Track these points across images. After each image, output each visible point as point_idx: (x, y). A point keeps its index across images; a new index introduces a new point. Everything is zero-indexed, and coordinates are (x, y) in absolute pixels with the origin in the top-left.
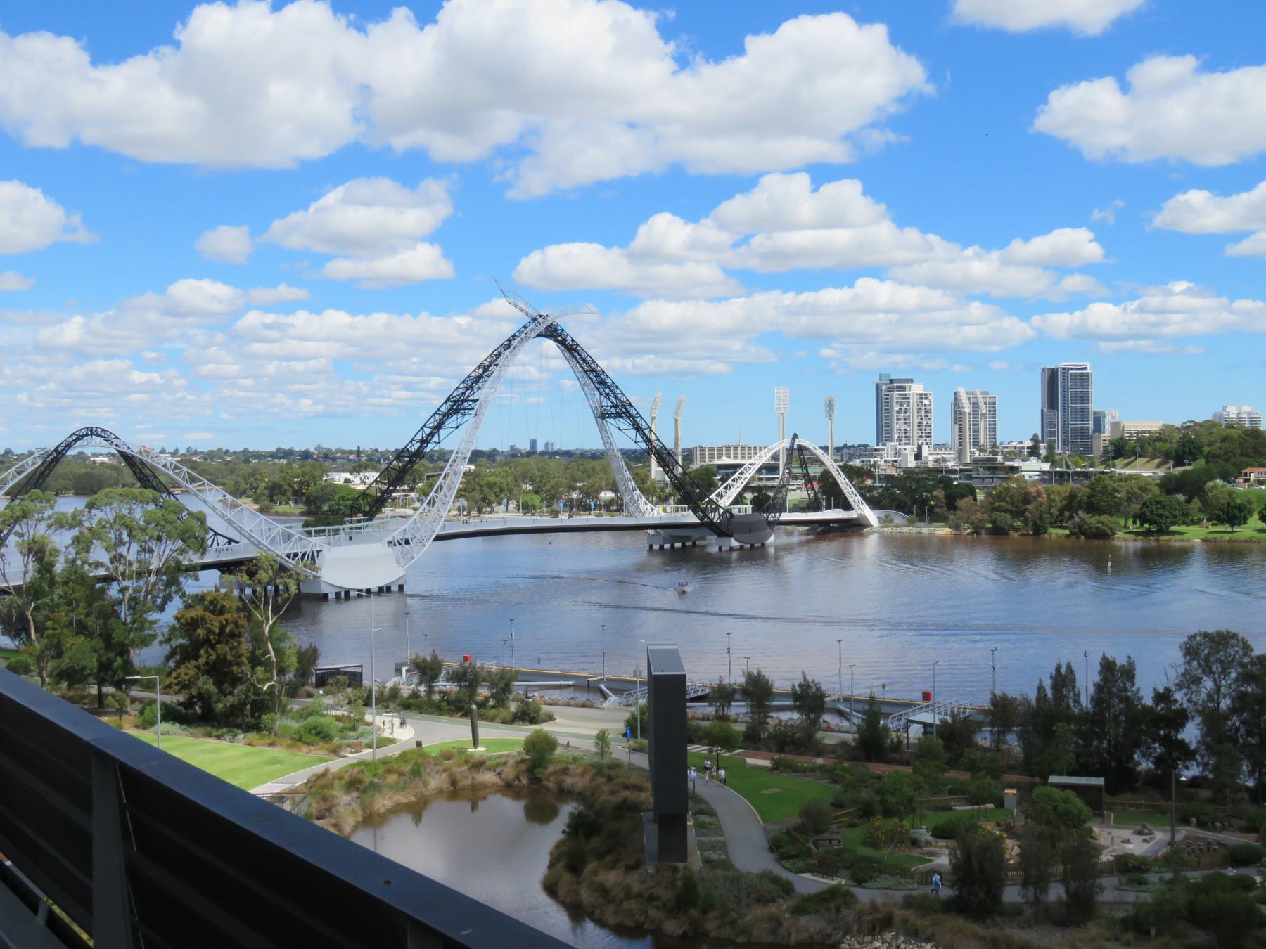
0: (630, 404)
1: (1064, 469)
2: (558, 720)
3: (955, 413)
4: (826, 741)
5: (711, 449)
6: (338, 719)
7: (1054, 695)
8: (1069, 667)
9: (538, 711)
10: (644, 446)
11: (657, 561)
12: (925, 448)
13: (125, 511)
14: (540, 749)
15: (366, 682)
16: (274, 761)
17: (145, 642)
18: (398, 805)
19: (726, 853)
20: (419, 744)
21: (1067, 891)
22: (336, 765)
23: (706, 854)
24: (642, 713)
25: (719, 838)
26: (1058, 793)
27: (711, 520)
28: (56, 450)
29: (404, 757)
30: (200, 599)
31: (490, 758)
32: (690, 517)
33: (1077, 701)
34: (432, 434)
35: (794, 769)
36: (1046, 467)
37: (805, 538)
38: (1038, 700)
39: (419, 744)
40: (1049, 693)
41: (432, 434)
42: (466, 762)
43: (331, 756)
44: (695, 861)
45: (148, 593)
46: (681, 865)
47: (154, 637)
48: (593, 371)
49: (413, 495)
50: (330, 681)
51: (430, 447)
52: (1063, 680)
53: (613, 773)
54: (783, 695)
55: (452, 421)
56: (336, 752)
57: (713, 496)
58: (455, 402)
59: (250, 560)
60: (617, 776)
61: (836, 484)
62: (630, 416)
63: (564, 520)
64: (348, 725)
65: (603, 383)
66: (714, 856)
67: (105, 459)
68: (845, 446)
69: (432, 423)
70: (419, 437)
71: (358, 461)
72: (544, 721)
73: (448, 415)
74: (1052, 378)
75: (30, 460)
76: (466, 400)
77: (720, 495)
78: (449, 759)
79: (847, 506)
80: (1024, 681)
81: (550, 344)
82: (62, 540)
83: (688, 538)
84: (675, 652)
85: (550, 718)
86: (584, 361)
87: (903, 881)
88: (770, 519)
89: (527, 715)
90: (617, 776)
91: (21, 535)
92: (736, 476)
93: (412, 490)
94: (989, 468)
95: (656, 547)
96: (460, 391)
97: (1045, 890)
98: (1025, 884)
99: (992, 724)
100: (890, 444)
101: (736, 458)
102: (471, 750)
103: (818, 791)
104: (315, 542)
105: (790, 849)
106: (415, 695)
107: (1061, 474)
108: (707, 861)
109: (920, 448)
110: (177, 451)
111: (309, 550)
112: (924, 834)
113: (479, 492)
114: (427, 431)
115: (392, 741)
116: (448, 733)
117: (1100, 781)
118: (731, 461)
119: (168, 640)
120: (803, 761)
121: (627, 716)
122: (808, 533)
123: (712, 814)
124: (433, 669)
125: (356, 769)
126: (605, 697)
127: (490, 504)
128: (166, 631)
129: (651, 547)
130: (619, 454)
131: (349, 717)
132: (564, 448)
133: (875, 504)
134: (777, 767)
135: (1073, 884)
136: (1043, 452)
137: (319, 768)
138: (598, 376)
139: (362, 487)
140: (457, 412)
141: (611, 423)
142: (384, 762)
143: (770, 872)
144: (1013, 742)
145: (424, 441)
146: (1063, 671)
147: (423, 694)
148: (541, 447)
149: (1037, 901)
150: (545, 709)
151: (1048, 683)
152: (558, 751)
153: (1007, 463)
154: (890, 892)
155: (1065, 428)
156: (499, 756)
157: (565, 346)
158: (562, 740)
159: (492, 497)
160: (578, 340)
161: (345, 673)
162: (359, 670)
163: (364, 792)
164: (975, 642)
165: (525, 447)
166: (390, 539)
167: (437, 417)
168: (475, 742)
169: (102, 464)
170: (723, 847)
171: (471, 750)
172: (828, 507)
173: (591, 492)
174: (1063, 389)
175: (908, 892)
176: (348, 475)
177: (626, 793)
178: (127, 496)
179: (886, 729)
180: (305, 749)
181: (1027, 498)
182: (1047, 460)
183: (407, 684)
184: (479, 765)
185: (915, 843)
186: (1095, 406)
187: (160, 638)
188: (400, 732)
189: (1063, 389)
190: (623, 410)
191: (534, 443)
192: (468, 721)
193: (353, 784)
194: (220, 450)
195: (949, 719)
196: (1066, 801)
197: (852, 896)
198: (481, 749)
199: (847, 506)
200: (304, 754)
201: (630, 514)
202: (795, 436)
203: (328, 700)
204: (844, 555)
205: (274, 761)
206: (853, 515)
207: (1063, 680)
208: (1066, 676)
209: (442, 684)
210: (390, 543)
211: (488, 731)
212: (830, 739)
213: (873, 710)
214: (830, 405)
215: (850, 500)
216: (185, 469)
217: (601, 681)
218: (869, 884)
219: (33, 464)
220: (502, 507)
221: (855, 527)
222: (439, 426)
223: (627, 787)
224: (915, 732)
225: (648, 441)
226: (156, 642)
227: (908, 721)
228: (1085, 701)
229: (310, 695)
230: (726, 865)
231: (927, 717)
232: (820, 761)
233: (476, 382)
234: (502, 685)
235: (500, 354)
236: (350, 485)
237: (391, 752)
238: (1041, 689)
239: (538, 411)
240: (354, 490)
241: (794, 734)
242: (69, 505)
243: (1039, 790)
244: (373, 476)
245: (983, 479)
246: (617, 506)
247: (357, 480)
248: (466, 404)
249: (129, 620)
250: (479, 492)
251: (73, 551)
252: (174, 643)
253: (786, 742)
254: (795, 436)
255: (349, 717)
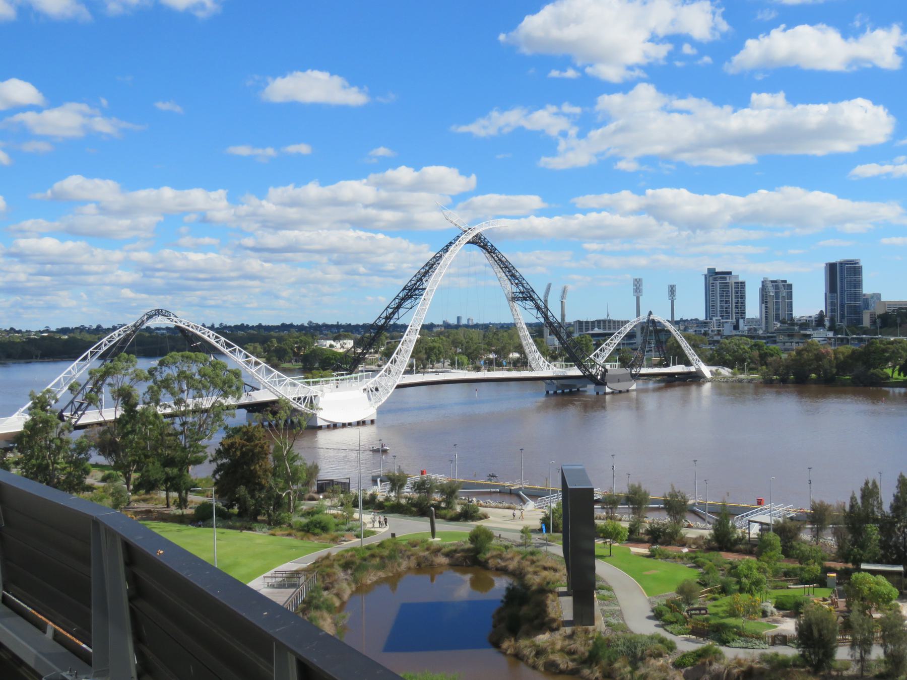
0: (533, 291)
1: (844, 336)
2: (491, 518)
3: (763, 296)
4: (689, 536)
5: (587, 322)
6: (335, 516)
7: (863, 503)
8: (874, 483)
9: (476, 511)
10: (542, 320)
11: (553, 400)
12: (741, 321)
13: (185, 369)
14: (480, 539)
15: (353, 490)
16: (292, 547)
17: (198, 462)
18: (381, 578)
19: (623, 620)
20: (393, 535)
21: (885, 652)
22: (335, 550)
23: (608, 619)
24: (553, 513)
25: (617, 608)
26: (870, 578)
27: (591, 374)
28: (134, 326)
29: (381, 545)
30: (237, 431)
31: (444, 546)
32: (575, 372)
33: (880, 508)
34: (393, 313)
35: (666, 557)
36: (831, 334)
37: (657, 385)
38: (852, 506)
39: (393, 535)
40: (859, 501)
41: (393, 313)
42: (428, 549)
43: (332, 544)
44: (600, 623)
45: (200, 426)
46: (591, 628)
47: (206, 457)
48: (506, 267)
49: (377, 356)
50: (328, 489)
51: (392, 322)
52: (870, 492)
53: (535, 558)
54: (655, 502)
55: (408, 304)
56: (335, 540)
57: (592, 356)
58: (410, 290)
59: (273, 402)
60: (538, 561)
61: (679, 347)
62: (533, 300)
63: (484, 374)
64: (341, 521)
65: (513, 276)
66: (613, 621)
67: (164, 332)
68: (682, 320)
69: (393, 305)
70: (384, 315)
71: (338, 331)
72: (481, 519)
73: (404, 299)
74: (832, 269)
75: (116, 332)
76: (417, 289)
77: (597, 356)
78: (415, 546)
79: (688, 363)
80: (839, 495)
81: (477, 251)
82: (140, 390)
83: (574, 386)
84: (583, 470)
85: (485, 517)
86: (500, 260)
87: (757, 643)
88: (633, 372)
89: (468, 515)
90: (538, 561)
91: (110, 385)
92: (608, 341)
93: (376, 352)
94: (789, 336)
95: (551, 392)
96: (413, 282)
97: (868, 652)
98: (853, 645)
99: (812, 523)
100: (714, 319)
101: (604, 329)
102: (431, 540)
103: (687, 574)
104: (313, 390)
105: (668, 616)
106: (387, 499)
107: (842, 339)
108: (608, 625)
109: (738, 321)
110: (213, 326)
111: (308, 395)
112: (770, 607)
113: (425, 356)
114: (390, 311)
115: (373, 533)
116: (412, 528)
117: (900, 568)
118: (601, 331)
119: (214, 460)
120: (671, 550)
121: (542, 516)
122: (659, 381)
123: (609, 589)
124: (399, 480)
125: (350, 553)
126: (524, 502)
127: (432, 362)
128: (214, 453)
129: (548, 392)
130: (524, 326)
131: (342, 515)
132: (481, 322)
133: (709, 361)
134: (652, 556)
135: (890, 647)
136: (827, 323)
137: (323, 552)
138: (510, 271)
139: (341, 351)
140: (411, 297)
141: (518, 305)
142: (368, 548)
143: (659, 635)
144: (830, 540)
145: (388, 318)
146: (870, 485)
147: (393, 499)
148: (464, 322)
149: (862, 660)
150: (482, 510)
151: (858, 495)
152: (494, 542)
153: (802, 332)
154: (747, 650)
155: (842, 306)
156: (451, 545)
157: (487, 250)
158: (496, 533)
159: (434, 358)
160: (496, 246)
161: (338, 483)
162: (347, 481)
163: (356, 570)
164: (432, 407)
165: (453, 321)
166: (365, 387)
167: (397, 301)
168: (433, 534)
169: (162, 334)
170: (620, 614)
171: (431, 540)
172: (674, 364)
173: (502, 352)
174: (842, 277)
175: (762, 651)
176: (332, 342)
177: (545, 573)
178: (187, 358)
179: (734, 527)
180: (312, 538)
181: (819, 357)
182: (830, 329)
183: (381, 491)
184: (437, 551)
185: (764, 614)
186: (868, 288)
187: (210, 458)
188: (377, 528)
189: (842, 277)
190: (526, 295)
191: (459, 319)
192: (428, 519)
193: (346, 566)
194: (243, 325)
195: (781, 520)
196: (877, 583)
197: (721, 653)
198: (437, 539)
199: (688, 363)
200: (314, 542)
201: (532, 370)
202: (650, 313)
203: (327, 503)
204: (685, 401)
205: (292, 547)
206: (692, 369)
207: (870, 492)
208: (872, 490)
209: (407, 491)
210: (365, 390)
211: (442, 526)
212: (691, 534)
213: (723, 516)
214: (672, 290)
215: (691, 358)
216: (223, 339)
217: (520, 489)
218: (733, 644)
219: (119, 335)
220: (440, 364)
221: (696, 378)
222: (398, 307)
223: (545, 568)
224: (755, 530)
225: (546, 317)
226: (206, 462)
227: (750, 521)
228: (886, 508)
229: (312, 499)
230: (625, 629)
231: (766, 519)
232: (685, 550)
233: (424, 276)
234: (450, 492)
235: (441, 256)
236: (334, 349)
237: (373, 541)
238: (853, 498)
239: (465, 295)
240: (336, 352)
241: (665, 530)
242: (144, 364)
243: (855, 576)
244: (350, 344)
245: (784, 343)
246: (522, 363)
247: (338, 346)
248: (417, 292)
249: (188, 445)
250: (425, 356)
251: (148, 397)
252: (219, 462)
253: (656, 536)
254: (650, 313)
255: (342, 515)
